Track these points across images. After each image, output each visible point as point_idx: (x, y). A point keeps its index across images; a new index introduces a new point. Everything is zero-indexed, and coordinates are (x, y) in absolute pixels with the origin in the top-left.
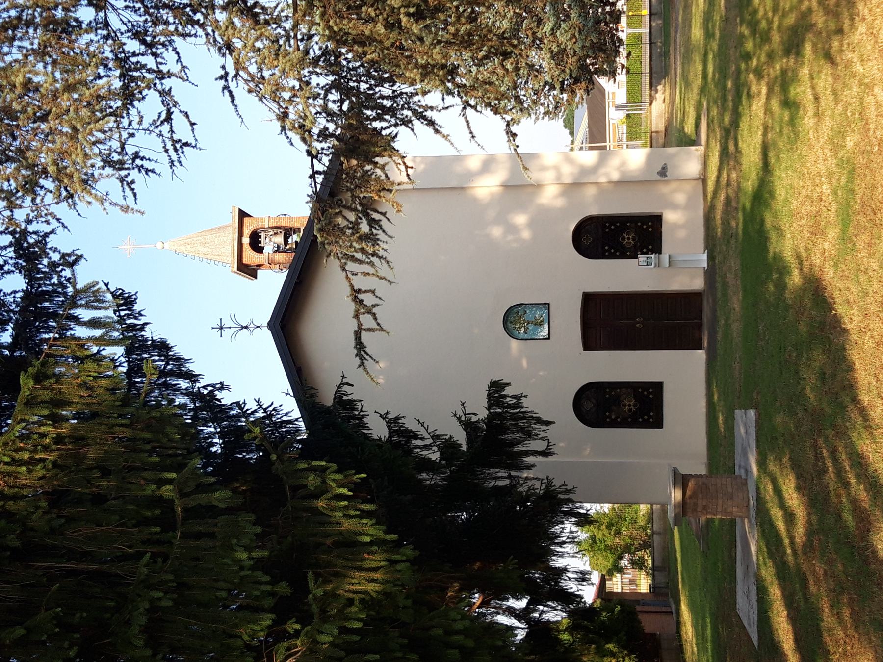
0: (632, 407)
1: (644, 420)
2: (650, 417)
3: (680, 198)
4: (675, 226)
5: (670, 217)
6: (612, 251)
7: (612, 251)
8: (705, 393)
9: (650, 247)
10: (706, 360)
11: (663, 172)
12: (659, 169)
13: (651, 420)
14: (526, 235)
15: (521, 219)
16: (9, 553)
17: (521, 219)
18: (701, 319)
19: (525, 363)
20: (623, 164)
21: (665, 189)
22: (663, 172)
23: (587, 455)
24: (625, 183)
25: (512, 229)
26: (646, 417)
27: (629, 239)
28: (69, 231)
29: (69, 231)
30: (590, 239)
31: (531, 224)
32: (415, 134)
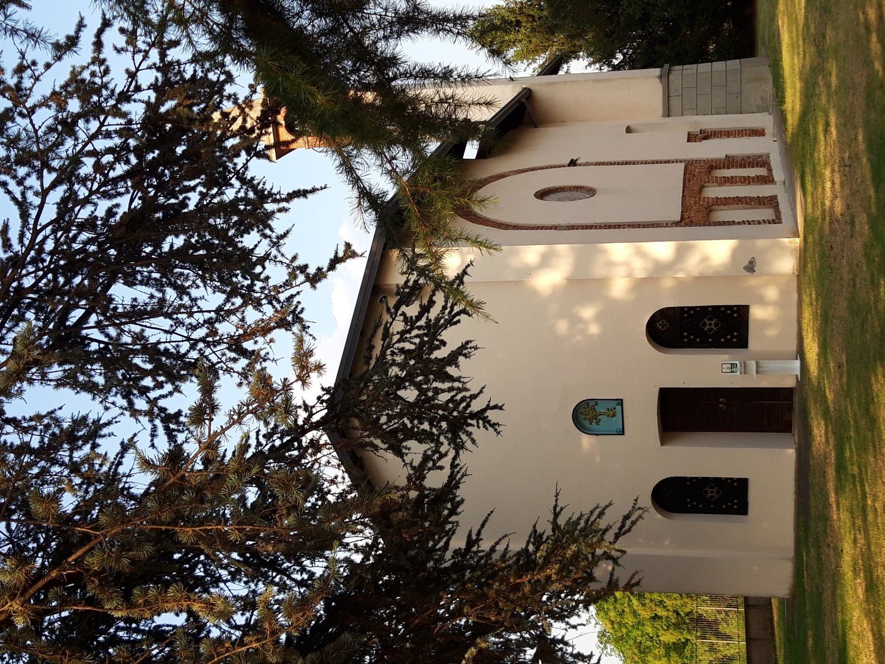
0: (713, 327)
1: (727, 340)
2: (734, 504)
3: (772, 293)
4: (765, 324)
5: (757, 313)
6: (692, 337)
7: (692, 337)
8: (793, 491)
9: (735, 334)
10: (796, 458)
11: (751, 268)
12: (746, 263)
13: (735, 507)
14: (594, 329)
15: (588, 312)
16: (111, 650)
17: (588, 312)
18: (792, 401)
19: (598, 459)
20: (705, 259)
21: (753, 281)
22: (751, 268)
23: (667, 549)
24: (703, 280)
25: (575, 321)
26: (729, 337)
27: (710, 325)
28: (135, 435)
29: (135, 435)
30: (663, 328)
31: (598, 318)
32: (481, 392)
